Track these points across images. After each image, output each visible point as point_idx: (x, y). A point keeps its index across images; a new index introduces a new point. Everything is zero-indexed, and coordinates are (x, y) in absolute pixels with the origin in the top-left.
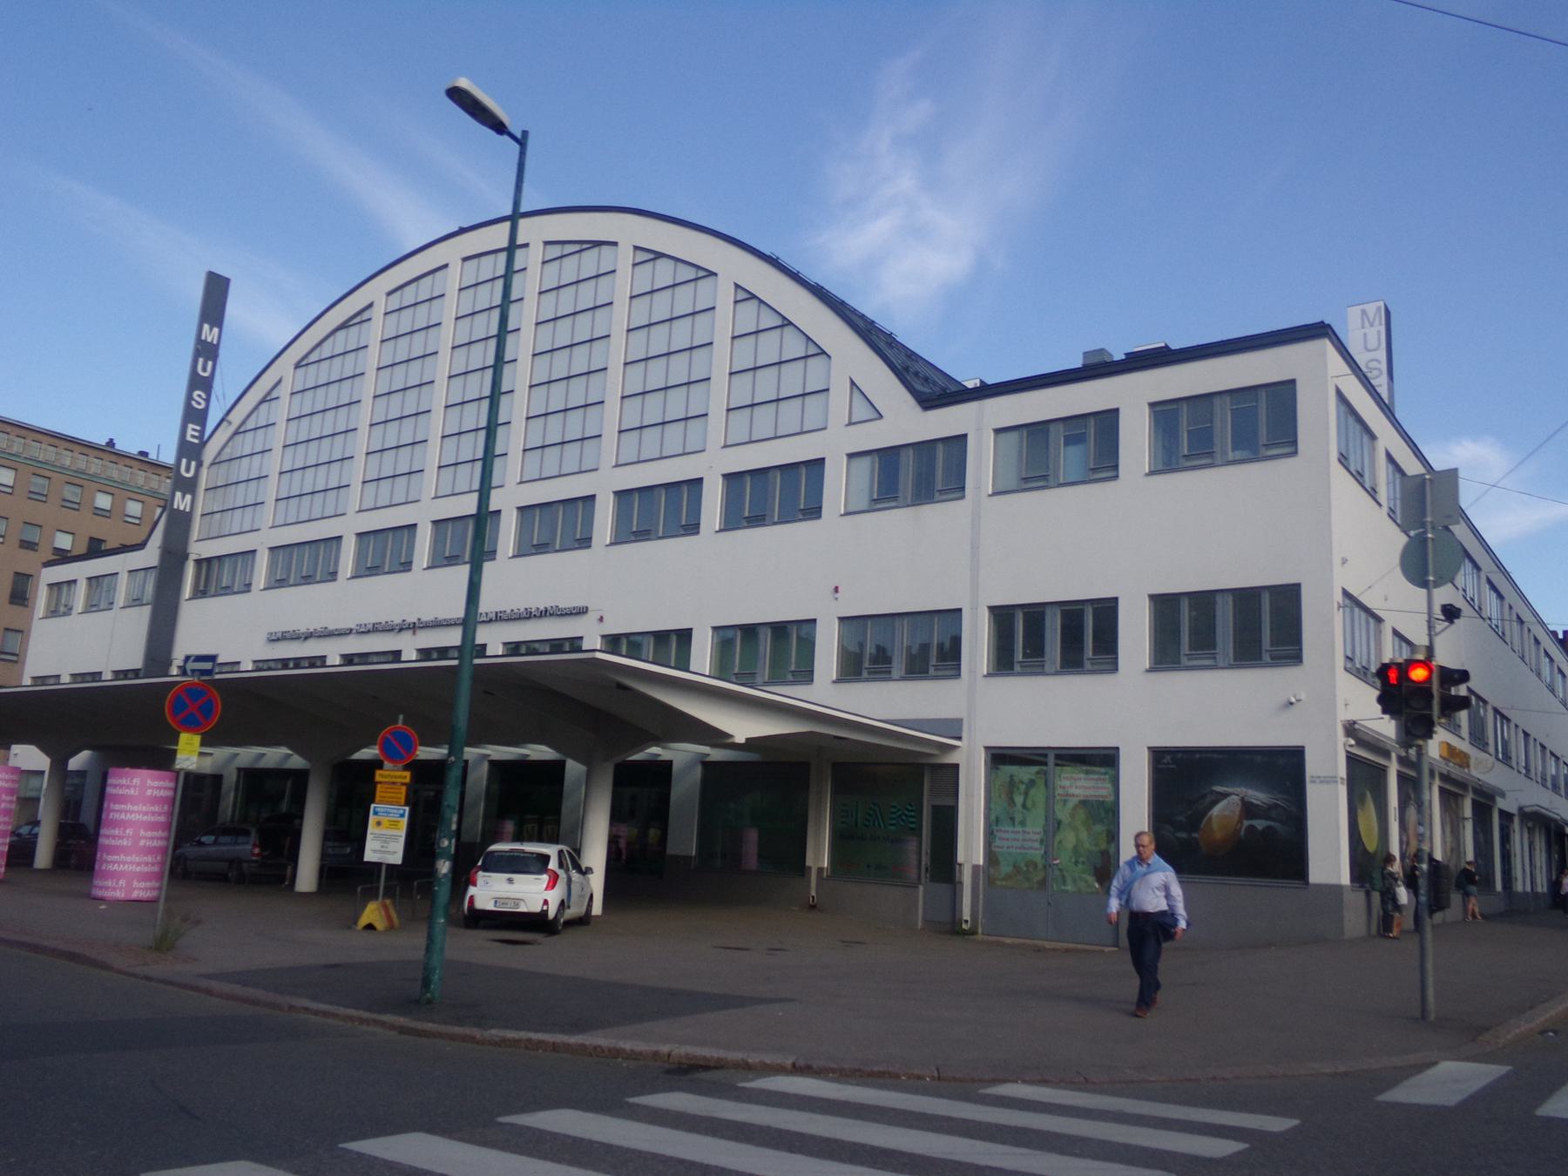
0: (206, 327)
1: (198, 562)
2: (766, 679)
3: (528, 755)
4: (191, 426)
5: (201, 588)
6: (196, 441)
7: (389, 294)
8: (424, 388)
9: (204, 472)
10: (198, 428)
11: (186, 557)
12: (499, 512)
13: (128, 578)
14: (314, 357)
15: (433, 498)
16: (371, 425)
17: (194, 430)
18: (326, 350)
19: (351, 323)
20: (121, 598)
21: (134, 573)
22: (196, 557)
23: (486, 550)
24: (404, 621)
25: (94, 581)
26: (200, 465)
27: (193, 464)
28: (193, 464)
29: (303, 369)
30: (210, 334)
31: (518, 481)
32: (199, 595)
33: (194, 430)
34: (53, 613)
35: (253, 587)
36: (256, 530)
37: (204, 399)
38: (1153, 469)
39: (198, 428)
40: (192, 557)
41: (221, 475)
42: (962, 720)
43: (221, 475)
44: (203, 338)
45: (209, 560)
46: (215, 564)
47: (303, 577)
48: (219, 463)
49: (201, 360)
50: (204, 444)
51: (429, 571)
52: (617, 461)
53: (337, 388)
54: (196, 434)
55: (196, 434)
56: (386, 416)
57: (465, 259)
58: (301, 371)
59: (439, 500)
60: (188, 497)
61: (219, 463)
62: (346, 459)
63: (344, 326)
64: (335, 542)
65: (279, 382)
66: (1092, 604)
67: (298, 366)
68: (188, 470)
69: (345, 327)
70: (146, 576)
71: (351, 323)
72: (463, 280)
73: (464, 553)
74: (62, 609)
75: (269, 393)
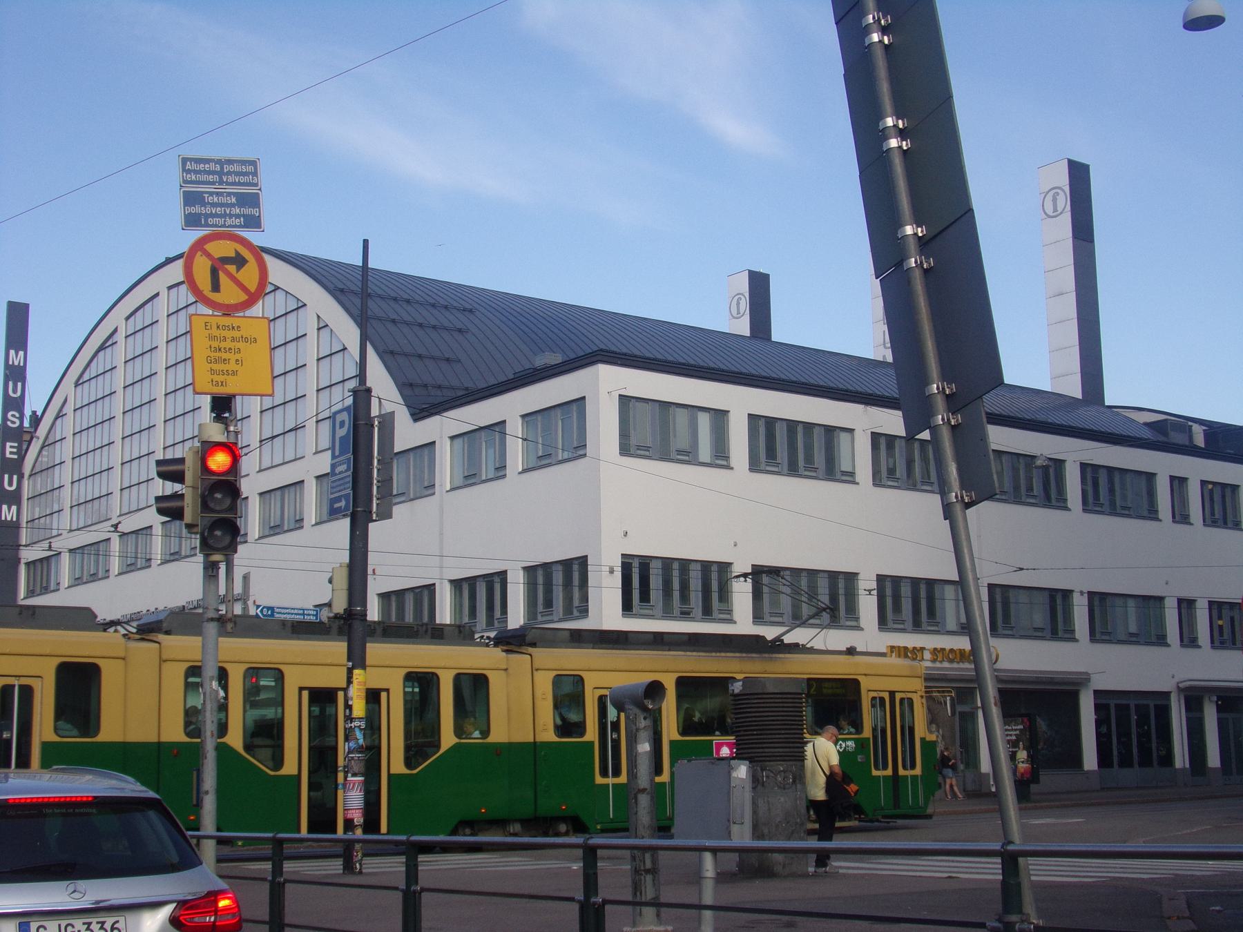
0: (12, 352)
1: (28, 564)
2: (561, 616)
3: (265, 715)
4: (8, 444)
5: (31, 588)
6: (16, 457)
7: (127, 318)
8: (300, 341)
9: (25, 482)
10: (16, 445)
11: (19, 560)
12: (247, 498)
13: (120, 540)
14: (86, 377)
15: (258, 472)
16: (318, 360)
17: (11, 447)
18: (93, 371)
19: (107, 345)
20: (115, 565)
21: (267, 496)
22: (25, 561)
23: (395, 492)
24: (148, 611)
25: (469, 437)
26: (21, 477)
27: (15, 477)
28: (15, 477)
29: (81, 386)
30: (16, 358)
31: (258, 469)
32: (30, 595)
33: (11, 447)
34: (273, 529)
35: (306, 523)
36: (300, 458)
37: (9, 420)
38: (525, 467)
39: (16, 445)
40: (23, 561)
41: (40, 484)
42: (1209, 601)
43: (40, 484)
44: (11, 363)
45: (34, 562)
46: (39, 565)
47: (271, 528)
48: (35, 474)
49: (11, 384)
50: (22, 458)
51: (318, 526)
52: (260, 467)
53: (284, 320)
54: (15, 450)
55: (15, 450)
56: (132, 431)
57: (170, 288)
58: (80, 388)
59: (320, 454)
60: (14, 508)
61: (35, 474)
62: (244, 418)
63: (102, 348)
64: (426, 451)
65: (66, 400)
66: (498, 576)
67: (77, 384)
68: (10, 484)
69: (102, 350)
70: (137, 538)
71: (107, 345)
72: (170, 308)
73: (409, 490)
74: (140, 563)
75: (61, 410)
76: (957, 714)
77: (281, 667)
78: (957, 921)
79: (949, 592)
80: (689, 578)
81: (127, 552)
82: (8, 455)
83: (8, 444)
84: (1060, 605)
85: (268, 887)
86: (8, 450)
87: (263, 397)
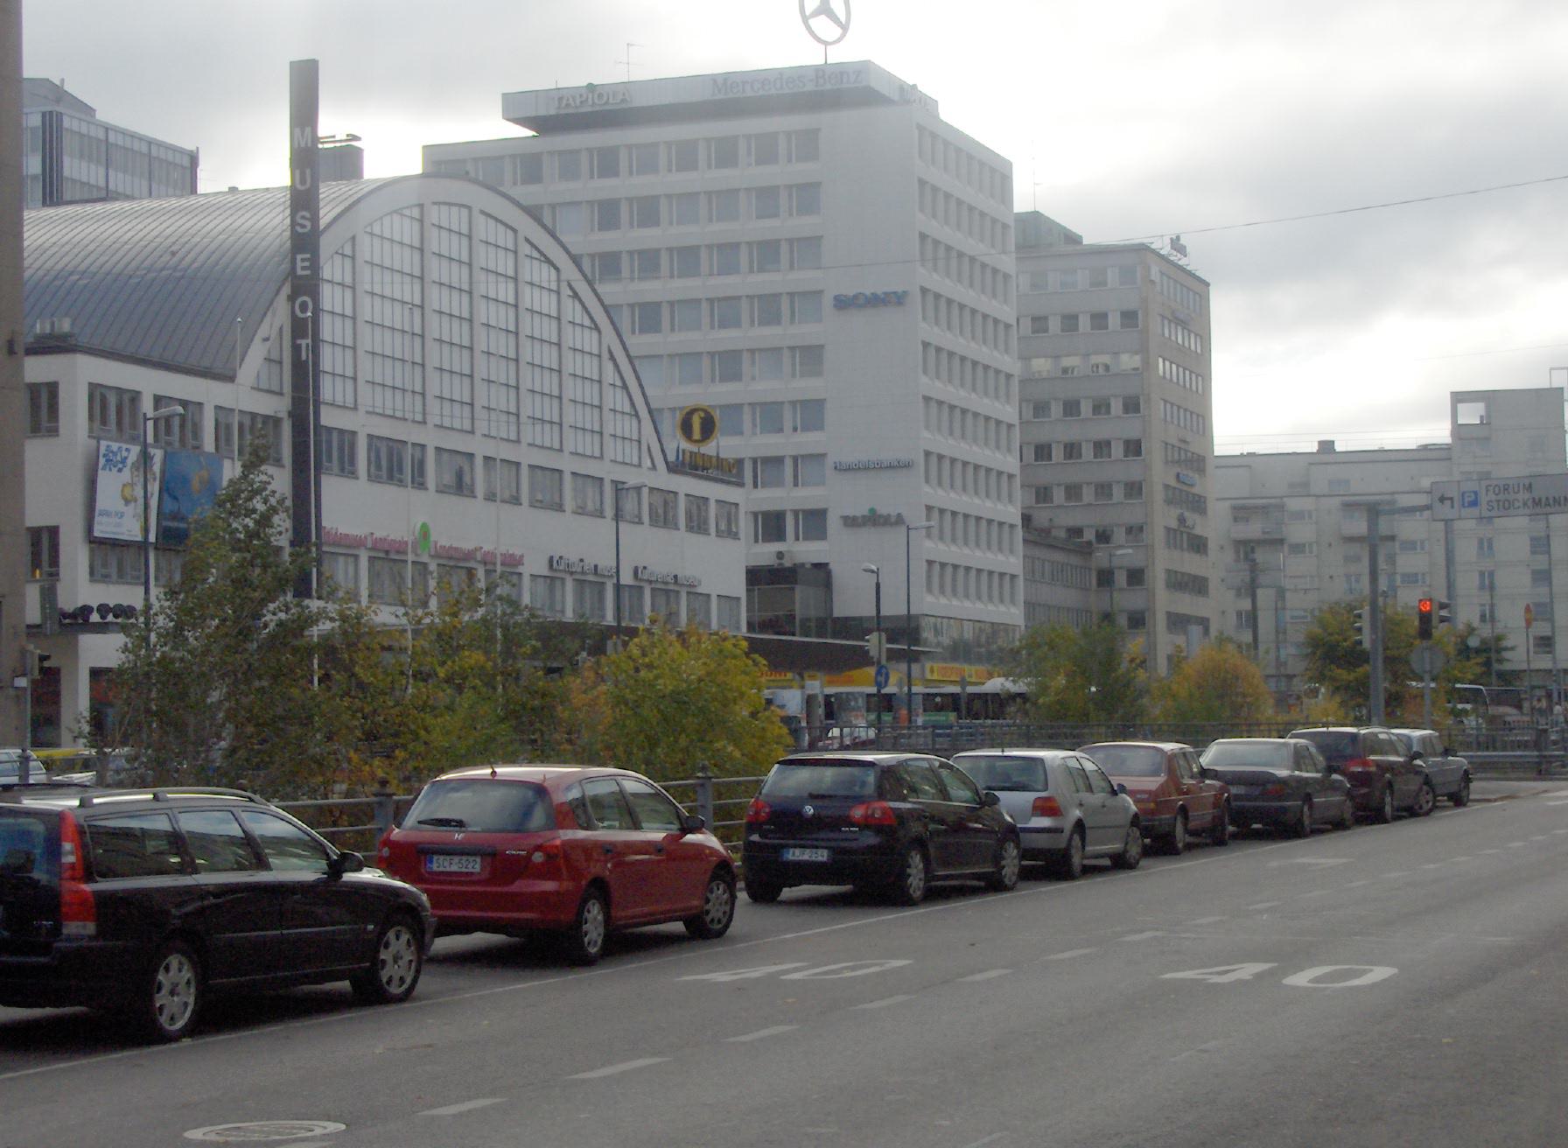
4: (299, 257)
6: (308, 272)
10: (308, 256)
17: (303, 260)
33: (303, 260)
39: (308, 256)
54: (307, 264)
55: (307, 264)
76: (1494, 674)
77: (232, 809)
78: (1370, 560)
79: (1315, 545)
80: (317, 311)
81: (414, 412)
82: (300, 272)
83: (299, 257)
84: (494, 773)
85: (1216, 448)
86: (299, 264)
87: (1550, 516)
